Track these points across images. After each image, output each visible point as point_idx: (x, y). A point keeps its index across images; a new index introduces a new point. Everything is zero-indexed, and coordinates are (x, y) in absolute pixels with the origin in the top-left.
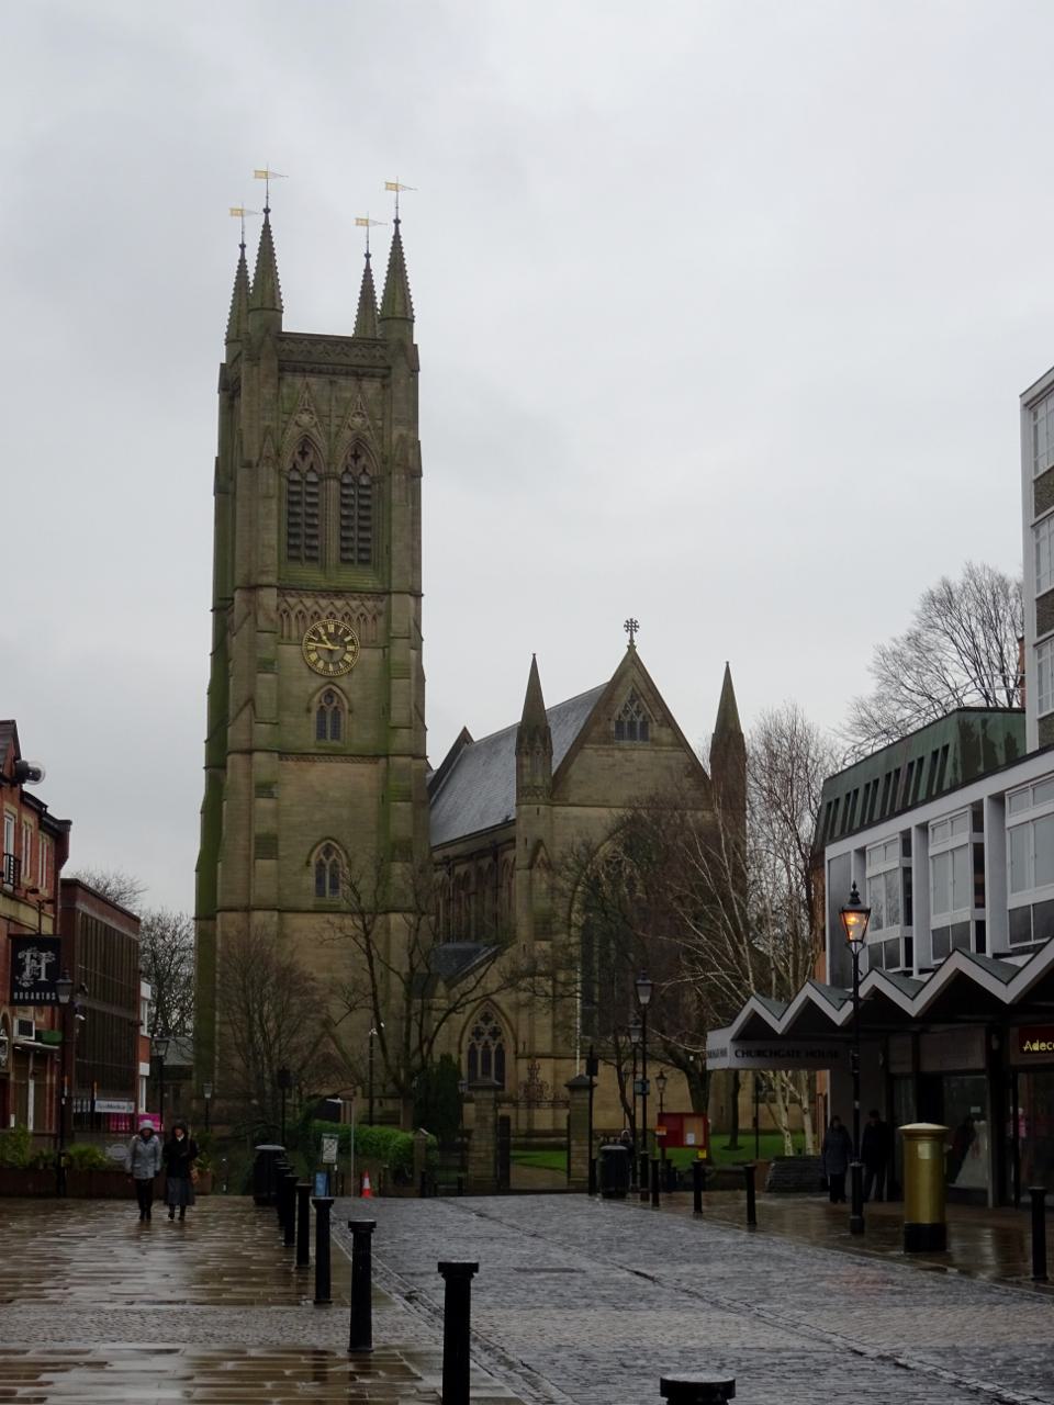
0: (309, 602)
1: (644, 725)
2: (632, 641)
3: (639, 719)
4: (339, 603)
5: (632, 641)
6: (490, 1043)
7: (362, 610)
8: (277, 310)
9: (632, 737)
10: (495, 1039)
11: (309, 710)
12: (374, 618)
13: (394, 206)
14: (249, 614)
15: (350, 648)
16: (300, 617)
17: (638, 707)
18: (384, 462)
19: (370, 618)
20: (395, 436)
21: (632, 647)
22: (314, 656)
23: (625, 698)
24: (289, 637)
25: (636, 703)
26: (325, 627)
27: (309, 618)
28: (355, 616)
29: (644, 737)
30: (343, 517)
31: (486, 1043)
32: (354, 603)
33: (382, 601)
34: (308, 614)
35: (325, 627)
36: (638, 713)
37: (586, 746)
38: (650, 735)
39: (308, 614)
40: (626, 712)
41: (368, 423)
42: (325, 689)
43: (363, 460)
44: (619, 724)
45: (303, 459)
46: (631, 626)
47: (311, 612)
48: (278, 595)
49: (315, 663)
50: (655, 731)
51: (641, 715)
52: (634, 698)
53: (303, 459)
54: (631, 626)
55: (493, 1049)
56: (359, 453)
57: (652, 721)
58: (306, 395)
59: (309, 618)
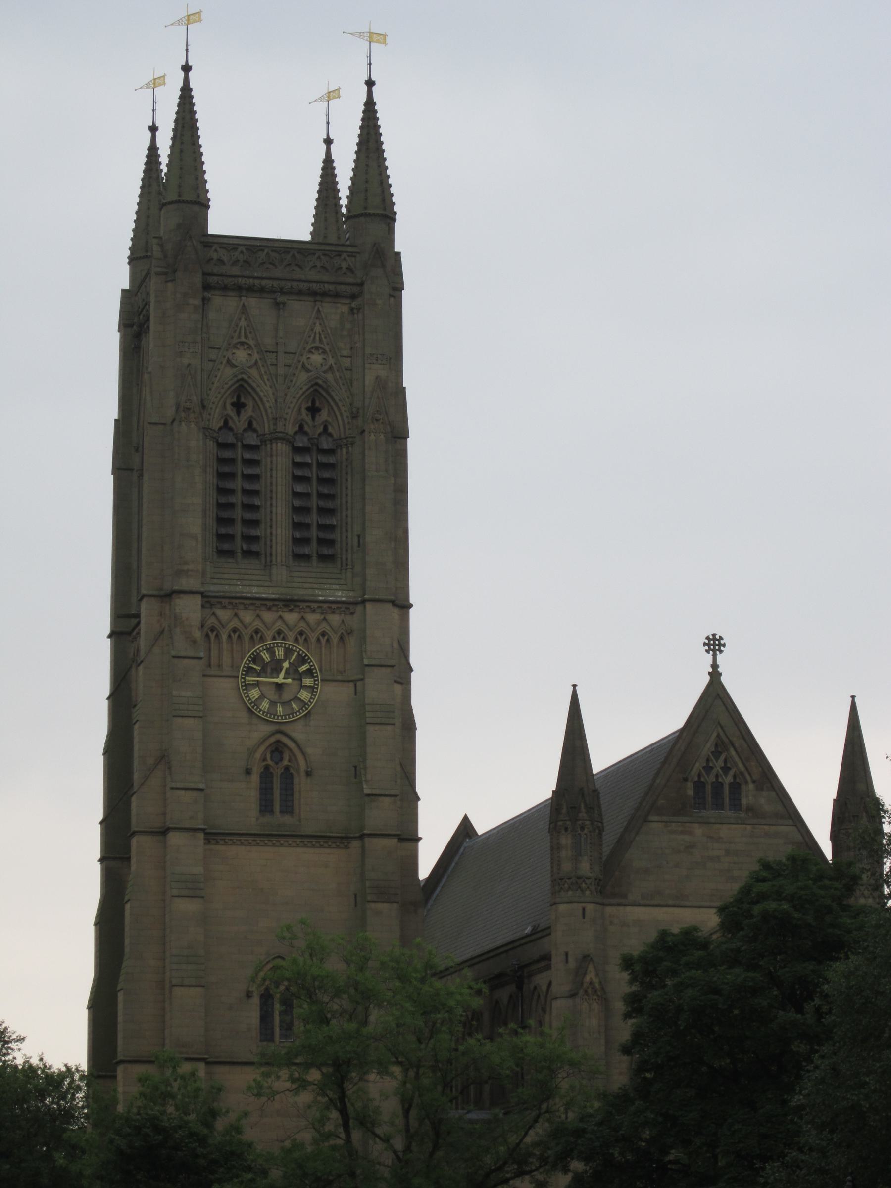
0: (248, 617)
1: (736, 787)
2: (715, 666)
3: (729, 779)
4: (291, 617)
5: (715, 666)
7: (324, 626)
8: (204, 205)
9: (719, 806)
11: (248, 772)
12: (341, 638)
13: (366, 61)
14: (162, 632)
15: (308, 681)
16: (235, 637)
17: (725, 761)
18: (355, 417)
19: (335, 639)
20: (369, 379)
21: (715, 674)
22: (255, 693)
23: (709, 747)
24: (220, 666)
25: (723, 757)
26: (271, 651)
27: (247, 638)
28: (313, 637)
29: (736, 805)
30: (296, 495)
32: (312, 618)
33: (352, 614)
34: (246, 634)
35: (271, 651)
36: (726, 769)
37: (651, 818)
38: (744, 802)
39: (246, 634)
40: (708, 769)
41: (331, 361)
42: (272, 740)
43: (324, 416)
44: (699, 786)
45: (238, 413)
46: (714, 644)
47: (250, 630)
48: (203, 607)
49: (257, 703)
50: (749, 796)
51: (732, 773)
52: (720, 748)
53: (238, 413)
54: (714, 644)
56: (317, 404)
57: (747, 782)
58: (243, 323)
59: (247, 638)
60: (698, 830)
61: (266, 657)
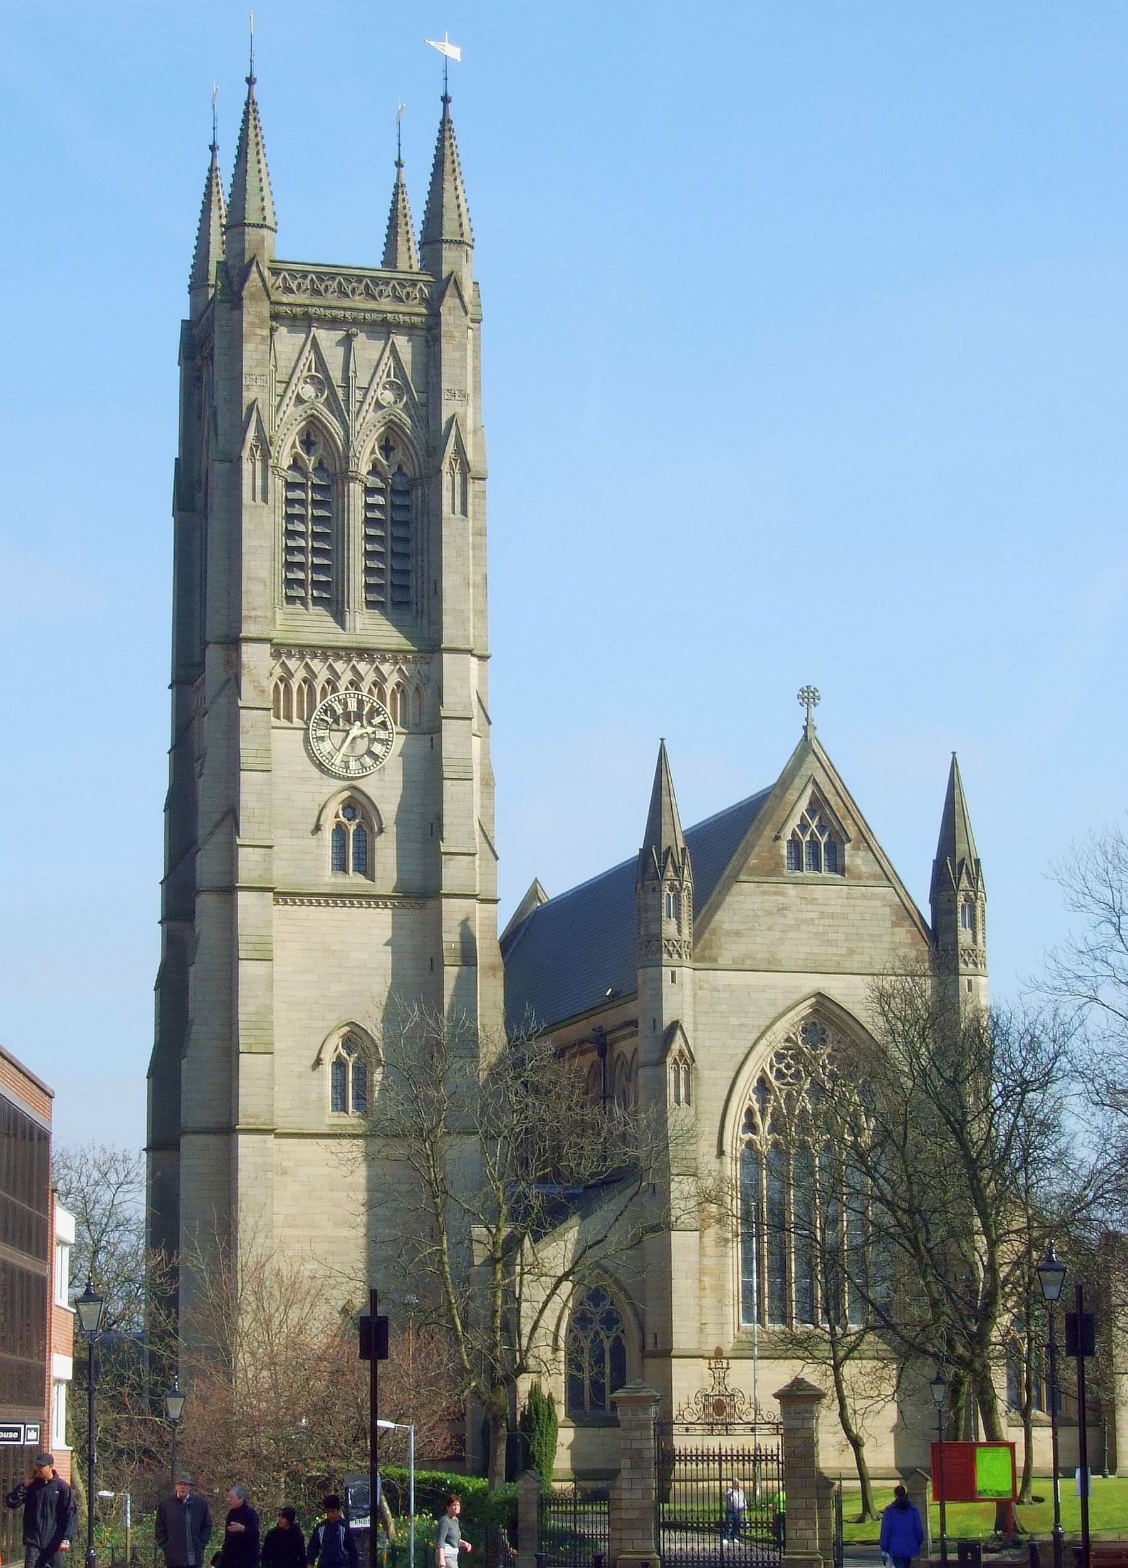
6: (602, 1335)
10: (609, 1329)
13: (442, 76)
14: (228, 680)
31: (597, 1333)
46: (809, 696)
54: (809, 696)
55: (607, 1345)
56: (392, 443)
60: (791, 890)
61: (339, 709)
